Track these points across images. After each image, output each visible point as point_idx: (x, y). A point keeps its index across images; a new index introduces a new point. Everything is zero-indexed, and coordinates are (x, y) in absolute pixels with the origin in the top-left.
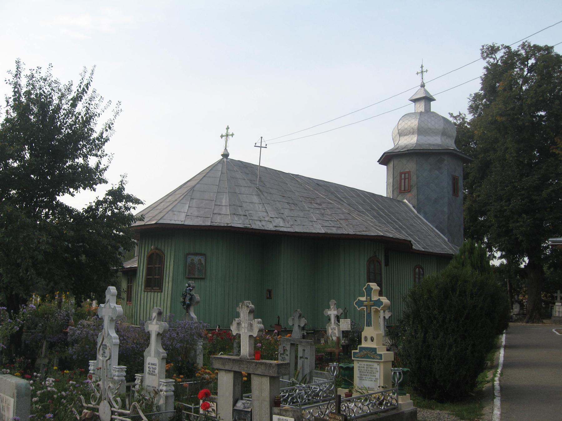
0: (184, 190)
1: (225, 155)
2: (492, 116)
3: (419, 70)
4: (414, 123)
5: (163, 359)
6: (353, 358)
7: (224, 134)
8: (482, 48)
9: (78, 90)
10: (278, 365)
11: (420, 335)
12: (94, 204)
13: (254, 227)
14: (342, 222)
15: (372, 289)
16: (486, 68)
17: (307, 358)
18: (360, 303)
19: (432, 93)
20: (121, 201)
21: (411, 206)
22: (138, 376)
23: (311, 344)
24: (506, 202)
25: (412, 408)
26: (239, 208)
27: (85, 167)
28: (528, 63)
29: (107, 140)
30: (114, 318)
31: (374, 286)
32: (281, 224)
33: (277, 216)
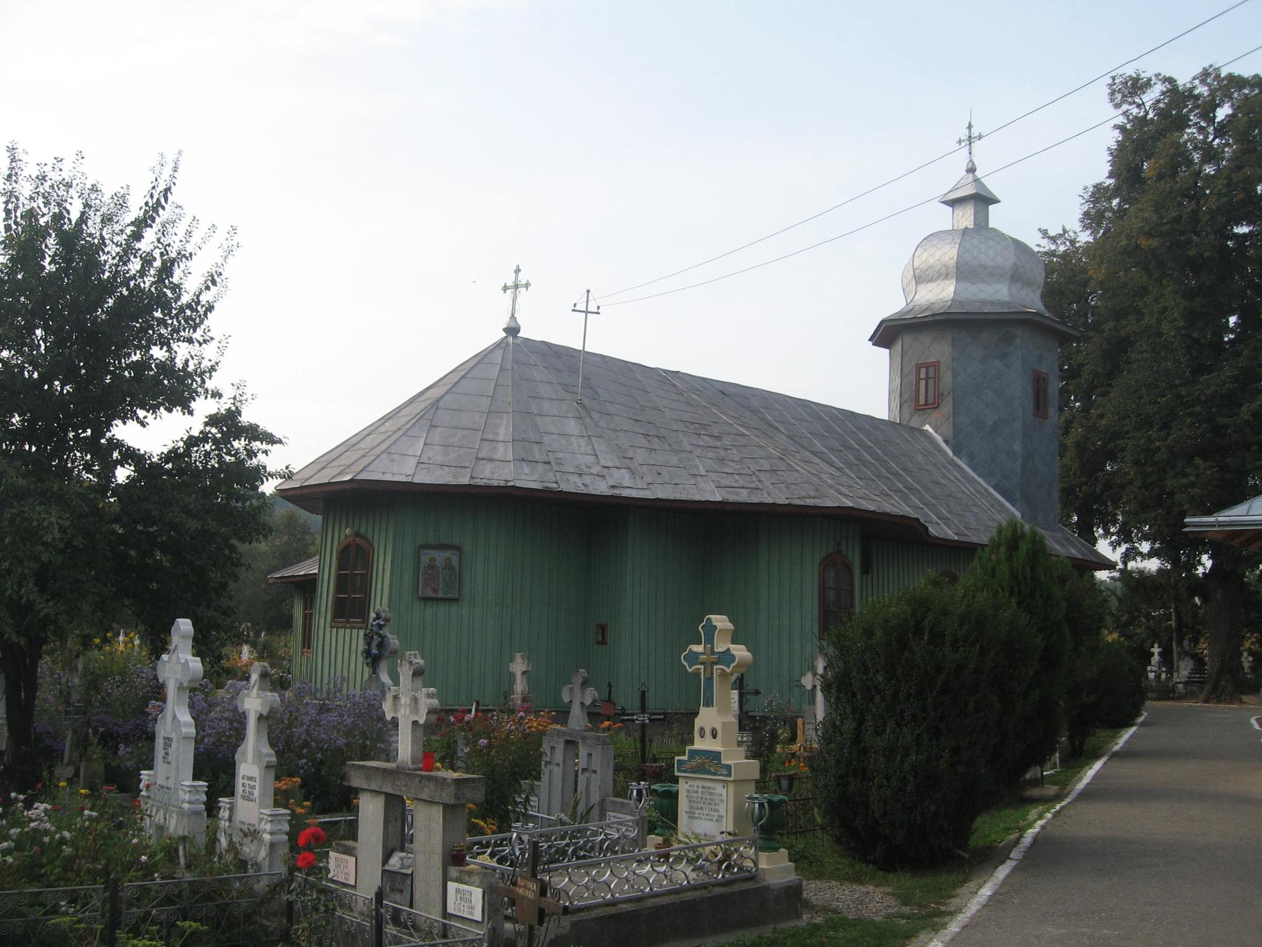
0: (418, 407)
1: (512, 330)
2: (1129, 237)
3: (964, 134)
4: (948, 254)
5: (267, 767)
6: (676, 773)
7: (510, 284)
8: (1110, 81)
9: (147, 204)
10: (457, 782)
11: (849, 726)
12: (181, 444)
13: (565, 487)
14: (762, 476)
15: (715, 627)
16: (1122, 128)
17: (595, 772)
18: (693, 658)
19: (993, 186)
20: (238, 438)
21: (939, 439)
22: (224, 801)
23: (604, 743)
24: (1161, 429)
25: (792, 877)
26: (535, 447)
27: (167, 368)
28: (1215, 117)
29: (210, 308)
30: (185, 685)
31: (721, 621)
32: (627, 483)
33: (618, 464)
